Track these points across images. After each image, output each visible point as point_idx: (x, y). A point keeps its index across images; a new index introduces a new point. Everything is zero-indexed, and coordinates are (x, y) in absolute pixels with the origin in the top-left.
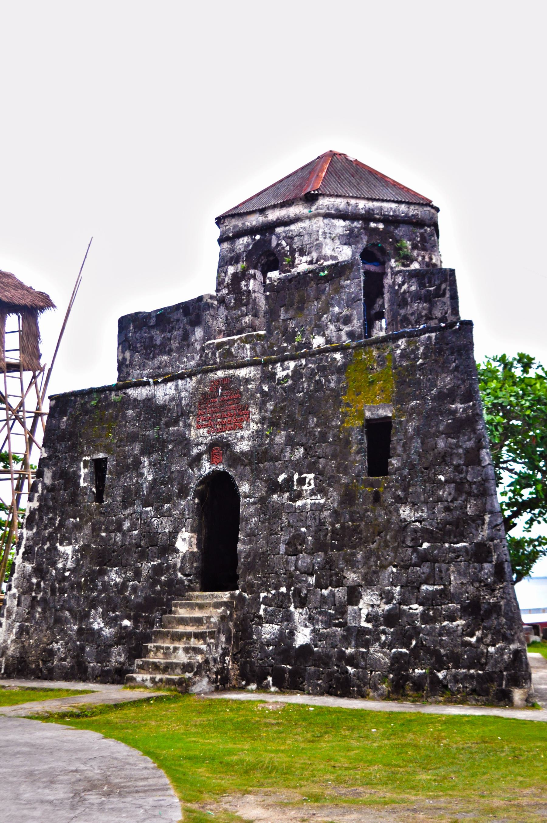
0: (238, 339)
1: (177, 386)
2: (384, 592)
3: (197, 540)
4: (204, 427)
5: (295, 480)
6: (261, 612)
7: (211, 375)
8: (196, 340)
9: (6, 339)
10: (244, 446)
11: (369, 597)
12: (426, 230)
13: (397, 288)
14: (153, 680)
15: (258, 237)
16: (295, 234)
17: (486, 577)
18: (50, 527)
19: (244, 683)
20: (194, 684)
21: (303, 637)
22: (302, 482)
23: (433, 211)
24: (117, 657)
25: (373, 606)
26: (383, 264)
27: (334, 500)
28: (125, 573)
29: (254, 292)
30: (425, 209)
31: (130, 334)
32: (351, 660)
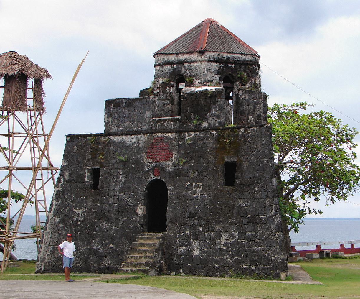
0: (168, 119)
1: (137, 138)
2: (231, 235)
3: (146, 209)
5: (194, 186)
6: (178, 242)
7: (154, 135)
8: (147, 117)
10: (170, 169)
11: (225, 236)
12: (253, 67)
13: (239, 96)
14: (132, 270)
15: (175, 66)
16: (193, 68)
17: (272, 230)
18: (69, 200)
19: (169, 272)
20: (150, 272)
21: (196, 252)
22: (196, 186)
23: (257, 58)
24: (107, 262)
25: (226, 240)
26: (233, 83)
27: (211, 195)
28: (111, 223)
29: (173, 93)
30: (254, 57)
31: (112, 109)
32: (217, 262)
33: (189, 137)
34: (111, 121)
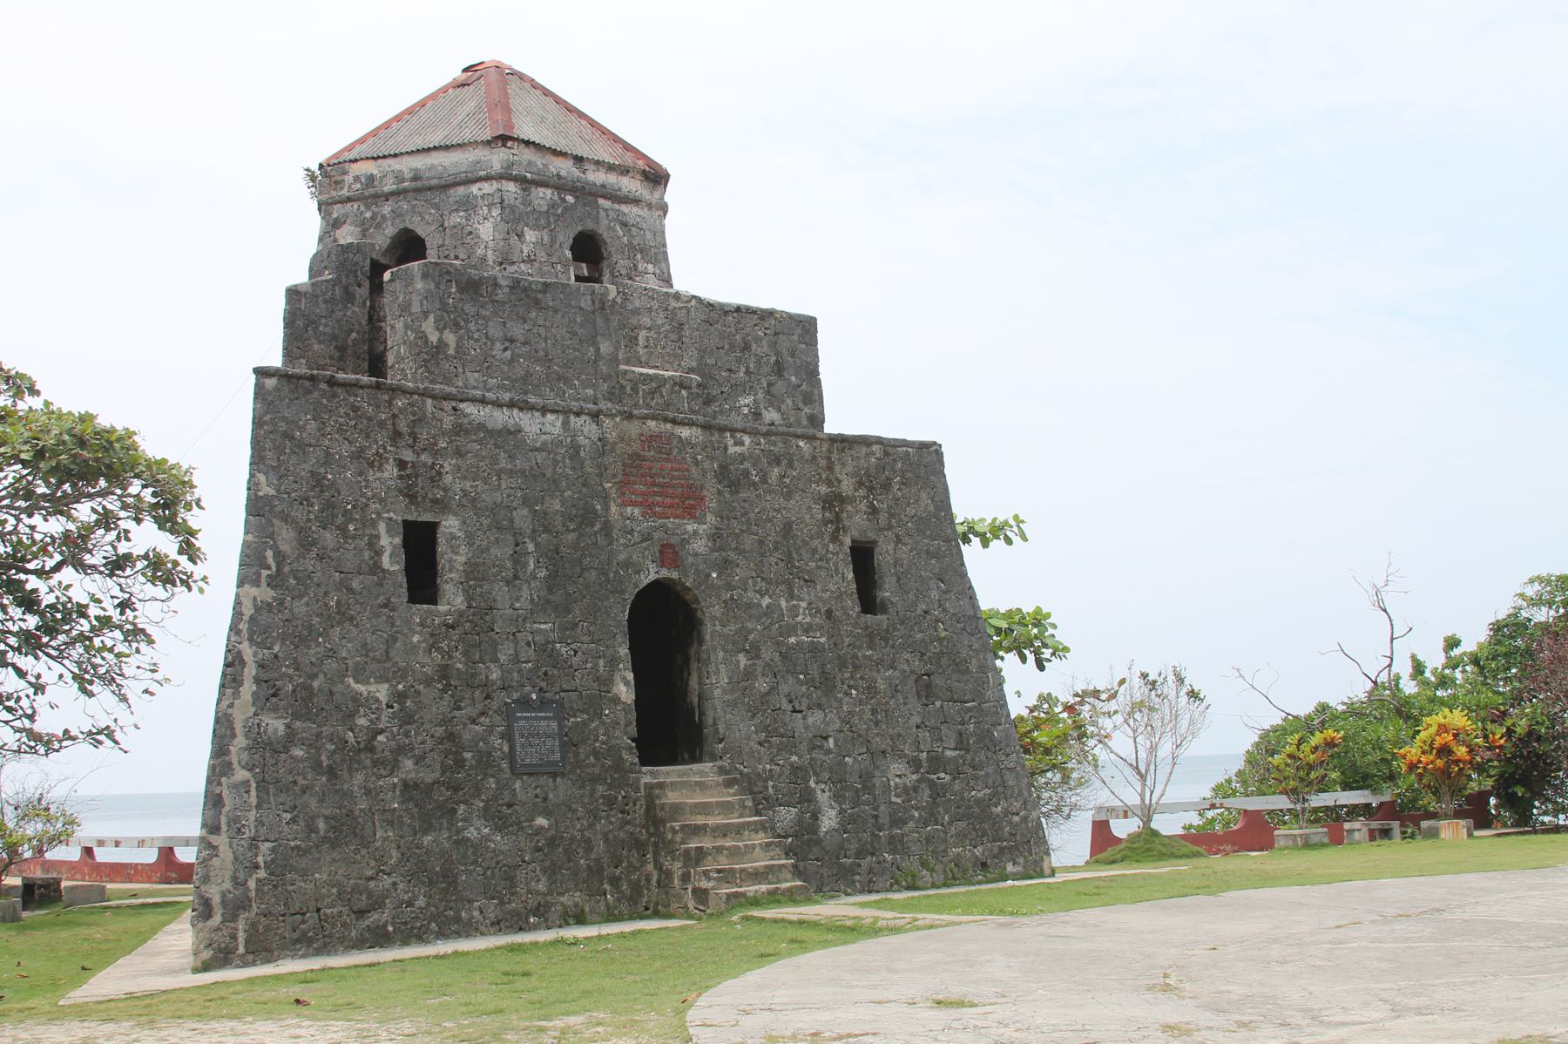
4: (634, 504)
9: (836, 432)
33: (737, 449)
34: (452, 345)
